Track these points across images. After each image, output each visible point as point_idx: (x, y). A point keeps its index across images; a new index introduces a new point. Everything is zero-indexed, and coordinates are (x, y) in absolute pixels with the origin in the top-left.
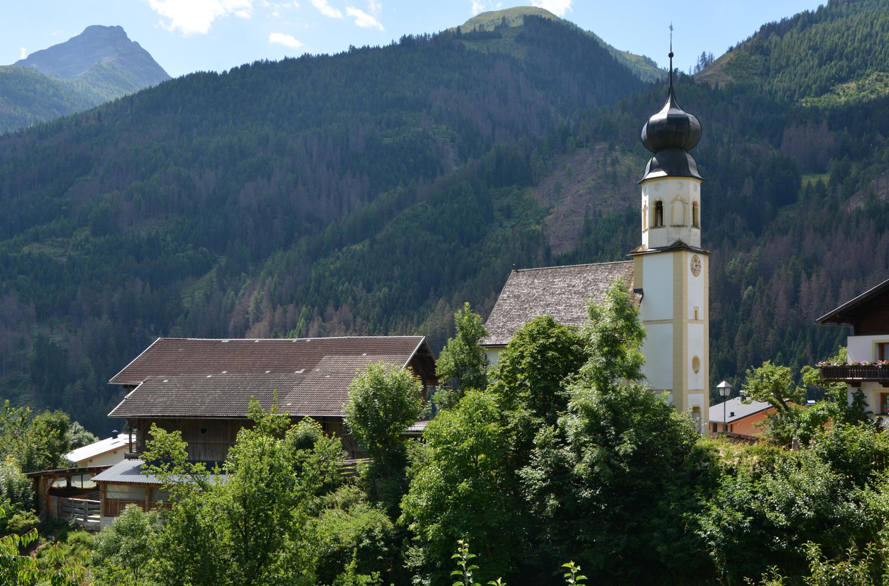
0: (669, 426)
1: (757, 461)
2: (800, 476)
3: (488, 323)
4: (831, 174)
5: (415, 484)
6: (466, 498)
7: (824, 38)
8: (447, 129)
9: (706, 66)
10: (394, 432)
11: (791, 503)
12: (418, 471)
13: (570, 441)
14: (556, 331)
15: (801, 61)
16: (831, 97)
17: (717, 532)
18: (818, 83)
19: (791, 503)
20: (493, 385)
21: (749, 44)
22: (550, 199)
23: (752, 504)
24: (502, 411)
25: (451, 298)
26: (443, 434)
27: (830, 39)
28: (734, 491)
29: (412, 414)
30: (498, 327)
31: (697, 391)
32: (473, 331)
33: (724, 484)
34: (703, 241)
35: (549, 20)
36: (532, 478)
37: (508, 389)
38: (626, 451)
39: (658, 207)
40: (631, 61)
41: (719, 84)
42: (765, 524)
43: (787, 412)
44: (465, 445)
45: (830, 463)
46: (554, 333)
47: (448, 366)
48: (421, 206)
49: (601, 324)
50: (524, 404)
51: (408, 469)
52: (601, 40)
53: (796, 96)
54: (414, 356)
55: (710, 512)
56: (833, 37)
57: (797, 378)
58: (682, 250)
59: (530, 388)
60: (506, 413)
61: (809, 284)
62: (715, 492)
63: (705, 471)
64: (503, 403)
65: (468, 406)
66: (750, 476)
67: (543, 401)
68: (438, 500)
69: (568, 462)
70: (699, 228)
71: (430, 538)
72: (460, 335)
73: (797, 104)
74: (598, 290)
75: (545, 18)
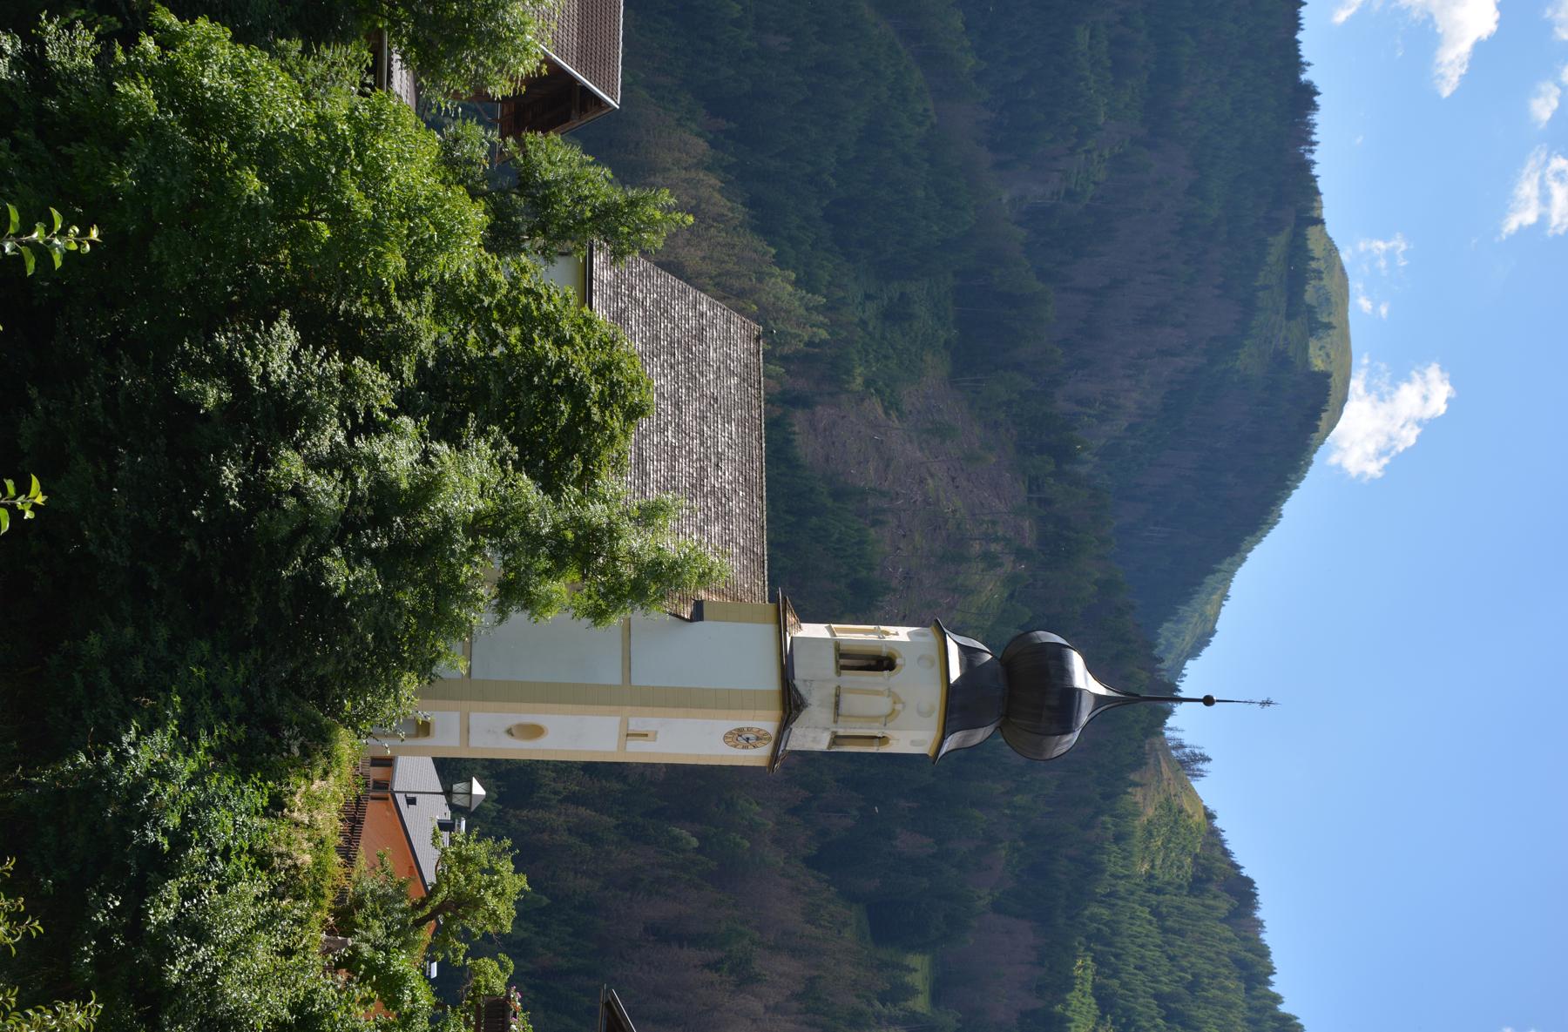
0: (386, 669)
1: (299, 862)
2: (262, 954)
3: (644, 264)
4: (930, 1014)
5: (258, 61)
6: (221, 184)
7: (1214, 1004)
8: (1095, 183)
9: (1181, 762)
10: (390, 17)
11: (200, 934)
12: (290, 71)
13: (358, 444)
14: (617, 424)
15: (1171, 958)
16: (1090, 1016)
17: (133, 771)
18: (1121, 991)
19: (200, 934)
20: (496, 268)
21: (1217, 854)
22: (919, 412)
23: (199, 850)
24: (434, 288)
25: (708, 169)
26: (380, 140)
27: (1210, 1016)
28: (231, 809)
29: (432, 66)
30: (632, 288)
31: (466, 731)
32: (626, 230)
33: (248, 789)
34: (806, 757)
35: (1316, 429)
36: (270, 351)
37: (486, 304)
38: (330, 571)
39: (882, 662)
40: (1206, 603)
41: (1139, 789)
42: (152, 876)
43: (410, 921)
44: (353, 193)
45: (291, 1019)
46: (612, 418)
47: (545, 164)
48: (926, 110)
49: (627, 526)
50: (448, 340)
51: (296, 46)
52: (1258, 541)
53: (1099, 947)
54: (573, 79)
55: (180, 756)
56: (1214, 1024)
57: (485, 946)
58: (784, 711)
59: (487, 357)
60: (429, 296)
61: (695, 967)
62: (229, 768)
63: (281, 747)
64: (452, 289)
65: (447, 207)
66: (265, 847)
67: (455, 385)
68: (217, 113)
69: (307, 436)
70: (829, 747)
71: (120, 89)
72: (618, 197)
73: (1082, 949)
74: (707, 520)
75: (1320, 419)
